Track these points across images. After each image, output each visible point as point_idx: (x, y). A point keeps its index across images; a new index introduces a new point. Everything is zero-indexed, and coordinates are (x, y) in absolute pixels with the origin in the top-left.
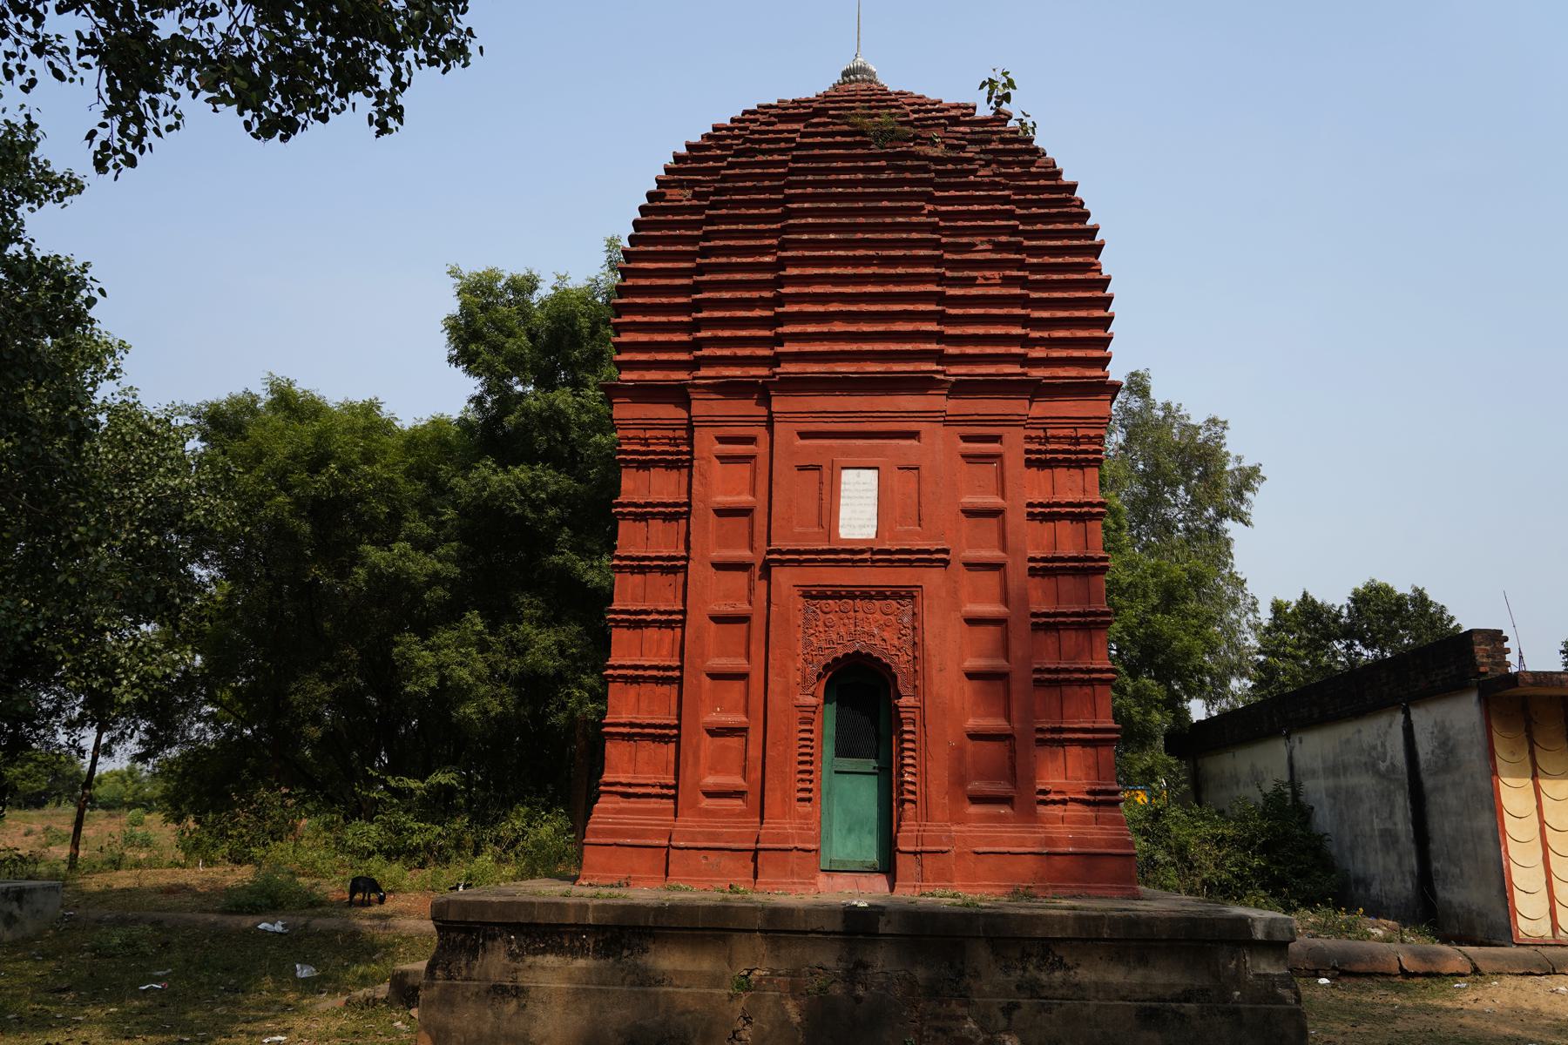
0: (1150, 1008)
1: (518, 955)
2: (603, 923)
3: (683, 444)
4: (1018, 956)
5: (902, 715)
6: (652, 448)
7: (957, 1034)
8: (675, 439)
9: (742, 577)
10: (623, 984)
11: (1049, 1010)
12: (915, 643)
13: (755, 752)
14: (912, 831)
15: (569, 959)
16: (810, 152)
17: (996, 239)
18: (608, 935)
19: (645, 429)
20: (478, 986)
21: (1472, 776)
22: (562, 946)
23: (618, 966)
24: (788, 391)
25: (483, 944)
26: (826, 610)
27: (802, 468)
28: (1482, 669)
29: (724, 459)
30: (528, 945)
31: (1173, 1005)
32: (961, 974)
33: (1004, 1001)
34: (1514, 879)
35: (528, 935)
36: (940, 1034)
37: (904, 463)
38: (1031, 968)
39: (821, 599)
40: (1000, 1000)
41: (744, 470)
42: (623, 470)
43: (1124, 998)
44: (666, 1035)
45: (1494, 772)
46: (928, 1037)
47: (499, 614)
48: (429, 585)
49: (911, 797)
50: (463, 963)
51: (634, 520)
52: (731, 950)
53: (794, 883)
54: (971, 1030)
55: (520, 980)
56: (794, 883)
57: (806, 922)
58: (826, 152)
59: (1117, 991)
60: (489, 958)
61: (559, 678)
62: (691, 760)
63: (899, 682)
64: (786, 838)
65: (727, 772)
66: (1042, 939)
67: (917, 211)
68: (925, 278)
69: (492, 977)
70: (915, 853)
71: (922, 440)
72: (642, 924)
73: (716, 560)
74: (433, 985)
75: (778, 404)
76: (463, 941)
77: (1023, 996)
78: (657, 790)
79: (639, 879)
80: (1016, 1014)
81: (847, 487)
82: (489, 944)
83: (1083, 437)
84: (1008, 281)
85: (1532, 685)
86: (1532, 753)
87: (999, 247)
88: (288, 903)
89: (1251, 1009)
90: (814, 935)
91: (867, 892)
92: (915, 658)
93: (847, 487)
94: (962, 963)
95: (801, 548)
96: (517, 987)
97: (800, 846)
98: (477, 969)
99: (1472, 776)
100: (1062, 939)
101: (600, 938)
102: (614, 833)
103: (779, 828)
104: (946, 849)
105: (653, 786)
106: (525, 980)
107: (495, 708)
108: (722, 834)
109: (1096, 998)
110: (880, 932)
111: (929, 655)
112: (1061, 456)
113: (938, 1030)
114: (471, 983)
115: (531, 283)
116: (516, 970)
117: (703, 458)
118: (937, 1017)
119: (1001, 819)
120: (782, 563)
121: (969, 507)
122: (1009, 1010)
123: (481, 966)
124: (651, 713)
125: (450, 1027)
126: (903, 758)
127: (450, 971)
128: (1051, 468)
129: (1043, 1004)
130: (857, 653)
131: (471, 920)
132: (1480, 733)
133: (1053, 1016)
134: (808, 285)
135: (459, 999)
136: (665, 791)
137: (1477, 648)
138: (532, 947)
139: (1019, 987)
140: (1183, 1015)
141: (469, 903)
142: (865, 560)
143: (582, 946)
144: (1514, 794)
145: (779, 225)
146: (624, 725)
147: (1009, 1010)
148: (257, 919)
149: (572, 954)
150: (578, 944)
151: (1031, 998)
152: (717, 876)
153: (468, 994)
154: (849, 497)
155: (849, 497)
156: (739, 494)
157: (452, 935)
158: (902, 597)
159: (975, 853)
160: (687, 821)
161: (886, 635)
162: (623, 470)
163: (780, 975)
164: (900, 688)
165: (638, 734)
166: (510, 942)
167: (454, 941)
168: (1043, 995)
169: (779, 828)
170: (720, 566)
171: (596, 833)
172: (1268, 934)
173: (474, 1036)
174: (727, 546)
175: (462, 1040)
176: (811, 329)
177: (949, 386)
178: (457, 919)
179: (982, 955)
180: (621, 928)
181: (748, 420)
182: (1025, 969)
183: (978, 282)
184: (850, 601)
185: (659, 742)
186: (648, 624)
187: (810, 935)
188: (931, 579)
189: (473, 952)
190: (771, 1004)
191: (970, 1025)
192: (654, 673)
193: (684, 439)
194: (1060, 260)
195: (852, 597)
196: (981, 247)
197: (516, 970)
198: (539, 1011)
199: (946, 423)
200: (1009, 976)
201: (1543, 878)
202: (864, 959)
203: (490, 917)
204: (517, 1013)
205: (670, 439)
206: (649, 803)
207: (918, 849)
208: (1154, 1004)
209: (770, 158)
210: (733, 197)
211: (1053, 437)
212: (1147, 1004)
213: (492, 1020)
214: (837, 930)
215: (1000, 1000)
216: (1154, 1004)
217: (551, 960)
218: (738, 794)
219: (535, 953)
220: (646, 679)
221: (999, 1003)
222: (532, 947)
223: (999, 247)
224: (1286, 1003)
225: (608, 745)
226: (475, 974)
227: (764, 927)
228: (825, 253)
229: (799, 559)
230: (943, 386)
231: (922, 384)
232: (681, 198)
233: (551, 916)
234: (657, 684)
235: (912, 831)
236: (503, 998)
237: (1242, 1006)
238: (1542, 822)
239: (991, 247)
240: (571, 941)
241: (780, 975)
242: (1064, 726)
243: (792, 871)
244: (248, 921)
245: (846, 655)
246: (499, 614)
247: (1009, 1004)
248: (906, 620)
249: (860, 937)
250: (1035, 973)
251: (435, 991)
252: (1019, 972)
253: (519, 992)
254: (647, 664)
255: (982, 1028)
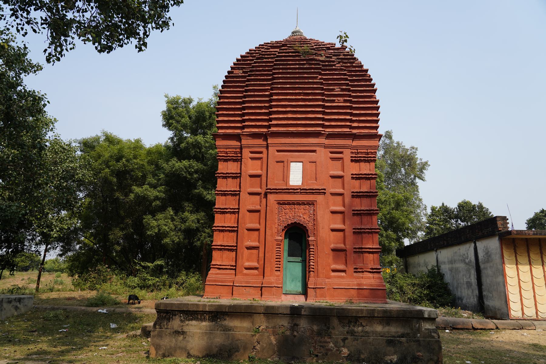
0: (390, 339)
1: (183, 321)
2: (211, 310)
3: (239, 154)
4: (347, 322)
5: (310, 243)
6: (228, 155)
7: (327, 348)
8: (236, 152)
9: (258, 197)
10: (218, 331)
11: (357, 340)
12: (314, 220)
13: (261, 255)
14: (313, 281)
15: (200, 322)
16: (281, 58)
17: (342, 87)
18: (213, 314)
19: (226, 149)
20: (170, 331)
21: (496, 264)
22: (198, 318)
23: (216, 325)
24: (273, 136)
25: (172, 317)
26: (285, 208)
27: (277, 162)
28: (500, 229)
29: (252, 159)
30: (187, 318)
31: (398, 338)
32: (329, 328)
33: (342, 337)
34: (510, 298)
35: (187, 314)
36: (321, 348)
37: (311, 160)
38: (351, 326)
39: (284, 205)
40: (341, 337)
41: (258, 162)
42: (219, 162)
43: (382, 336)
44: (232, 347)
45: (504, 263)
46: (317, 348)
47: (178, 209)
48: (154, 200)
49: (313, 270)
50: (165, 323)
51: (223, 179)
52: (253, 319)
53: (274, 298)
54: (332, 346)
55: (184, 329)
56: (274, 298)
57: (278, 310)
58: (286, 58)
59: (380, 334)
60: (174, 322)
61: (197, 230)
62: (240, 258)
63: (309, 232)
64: (272, 283)
65: (253, 261)
66: (355, 317)
67: (316, 78)
68: (318, 100)
69: (175, 328)
70: (314, 288)
71: (317, 153)
72: (224, 311)
73: (249, 192)
74: (155, 330)
75: (270, 141)
76: (165, 316)
77: (349, 335)
78: (229, 267)
79: (223, 296)
80: (346, 341)
81: (292, 168)
82: (174, 317)
83: (370, 152)
84: (345, 101)
85: (516, 234)
86: (516, 257)
87: (343, 90)
88: (108, 303)
89: (423, 340)
90: (280, 315)
91: (298, 301)
92: (314, 224)
93: (292, 168)
94: (329, 324)
95: (277, 188)
96: (183, 331)
97: (276, 286)
98: (170, 325)
99: (496, 264)
100: (360, 317)
101: (210, 315)
102: (215, 281)
103: (270, 280)
104: (324, 287)
105: (228, 266)
106: (185, 329)
107: (177, 240)
108: (251, 281)
109: (372, 336)
110: (302, 314)
111: (319, 223)
112: (362, 159)
113: (321, 346)
114: (168, 330)
115: (190, 101)
116: (183, 326)
117: (245, 158)
118: (320, 342)
119: (342, 277)
120: (271, 193)
121: (332, 175)
122: (344, 340)
123: (171, 324)
124: (227, 242)
125: (161, 344)
126: (310, 257)
127: (161, 326)
128: (359, 162)
129: (355, 338)
130: (295, 223)
131: (168, 309)
132: (499, 250)
133: (358, 342)
134: (280, 102)
135: (164, 335)
136: (232, 267)
137: (498, 222)
138: (188, 318)
139: (347, 332)
140: (401, 342)
141: (167, 304)
142: (298, 192)
143: (204, 318)
144: (510, 270)
145: (271, 82)
146: (219, 246)
147: (344, 340)
148: (98, 308)
149: (201, 321)
150: (203, 317)
151: (351, 336)
152: (249, 295)
153: (167, 334)
154: (293, 172)
155: (293, 172)
156: (257, 170)
157: (162, 314)
158: (310, 204)
159: (333, 288)
160: (239, 277)
161: (305, 217)
162: (219, 162)
163: (269, 328)
164: (309, 234)
165: (223, 248)
166: (181, 317)
167: (162, 316)
168: (355, 335)
169: (270, 280)
170: (250, 194)
171: (209, 281)
172: (429, 315)
173: (169, 347)
174: (253, 187)
175: (165, 349)
176: (281, 116)
177: (326, 135)
178: (163, 309)
179: (335, 322)
180: (217, 312)
181: (260, 146)
182: (349, 326)
183: (336, 101)
184: (293, 206)
185: (230, 251)
186: (227, 213)
187: (279, 315)
188: (319, 198)
189: (169, 320)
190: (266, 337)
191: (331, 345)
192: (229, 229)
193: (239, 152)
194: (363, 94)
195: (294, 204)
196: (337, 90)
197: (183, 326)
198: (190, 339)
199: (325, 147)
200: (344, 329)
201: (519, 298)
202: (297, 323)
203: (174, 309)
204: (183, 340)
205: (235, 152)
206: (227, 271)
207: (315, 287)
208: (391, 338)
209: (268, 60)
210: (256, 73)
211: (360, 152)
212: (389, 338)
213: (175, 342)
214: (288, 313)
215: (341, 337)
216: (391, 338)
217: (194, 322)
218: (256, 268)
219: (189, 320)
220: (226, 231)
221: (341, 338)
222: (188, 318)
223: (343, 90)
224: (435, 338)
225: (213, 252)
226: (169, 327)
227: (264, 312)
228: (286, 91)
229: (277, 191)
230: (324, 135)
231: (317, 135)
232: (239, 73)
233: (194, 308)
234: (230, 232)
235: (313, 281)
236: (178, 335)
237: (420, 339)
238: (519, 279)
239: (340, 90)
240: (201, 316)
241: (269, 328)
242: (363, 247)
243: (273, 294)
244: (95, 309)
245: (292, 223)
246: (178, 209)
247: (344, 338)
248: (311, 212)
249: (296, 316)
250: (353, 328)
251: (156, 333)
252: (347, 328)
253: (183, 333)
254: (226, 226)
255: (335, 346)
